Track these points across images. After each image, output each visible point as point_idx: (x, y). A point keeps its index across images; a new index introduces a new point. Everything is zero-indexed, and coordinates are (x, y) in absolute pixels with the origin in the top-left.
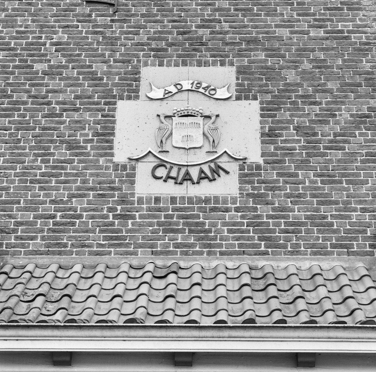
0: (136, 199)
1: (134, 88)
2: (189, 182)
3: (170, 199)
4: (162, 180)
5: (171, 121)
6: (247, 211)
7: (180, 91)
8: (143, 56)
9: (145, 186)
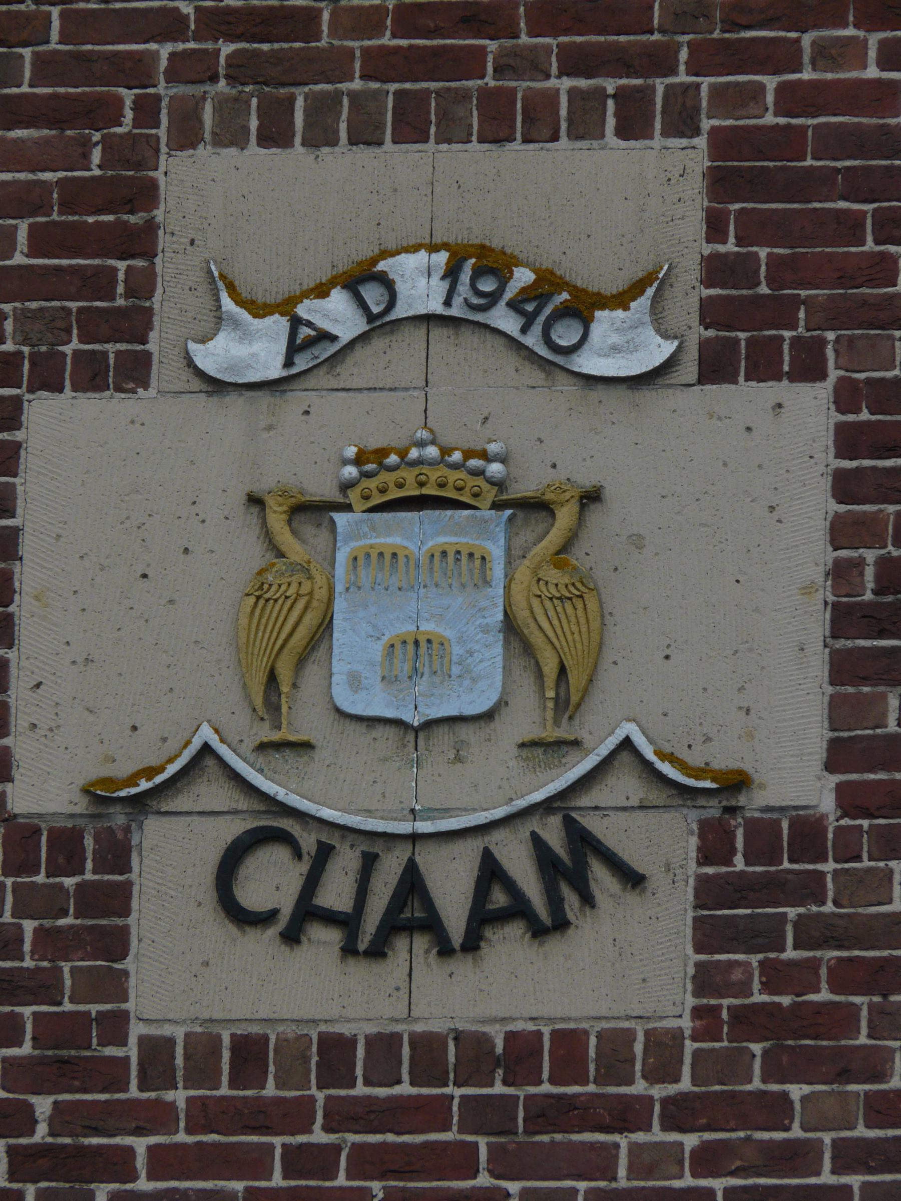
0: (132, 1051)
1: (120, 302)
2: (421, 942)
3: (314, 1049)
4: (273, 932)
5: (325, 534)
6: (732, 1124)
7: (380, 325)
8: (172, 76)
9: (189, 971)
